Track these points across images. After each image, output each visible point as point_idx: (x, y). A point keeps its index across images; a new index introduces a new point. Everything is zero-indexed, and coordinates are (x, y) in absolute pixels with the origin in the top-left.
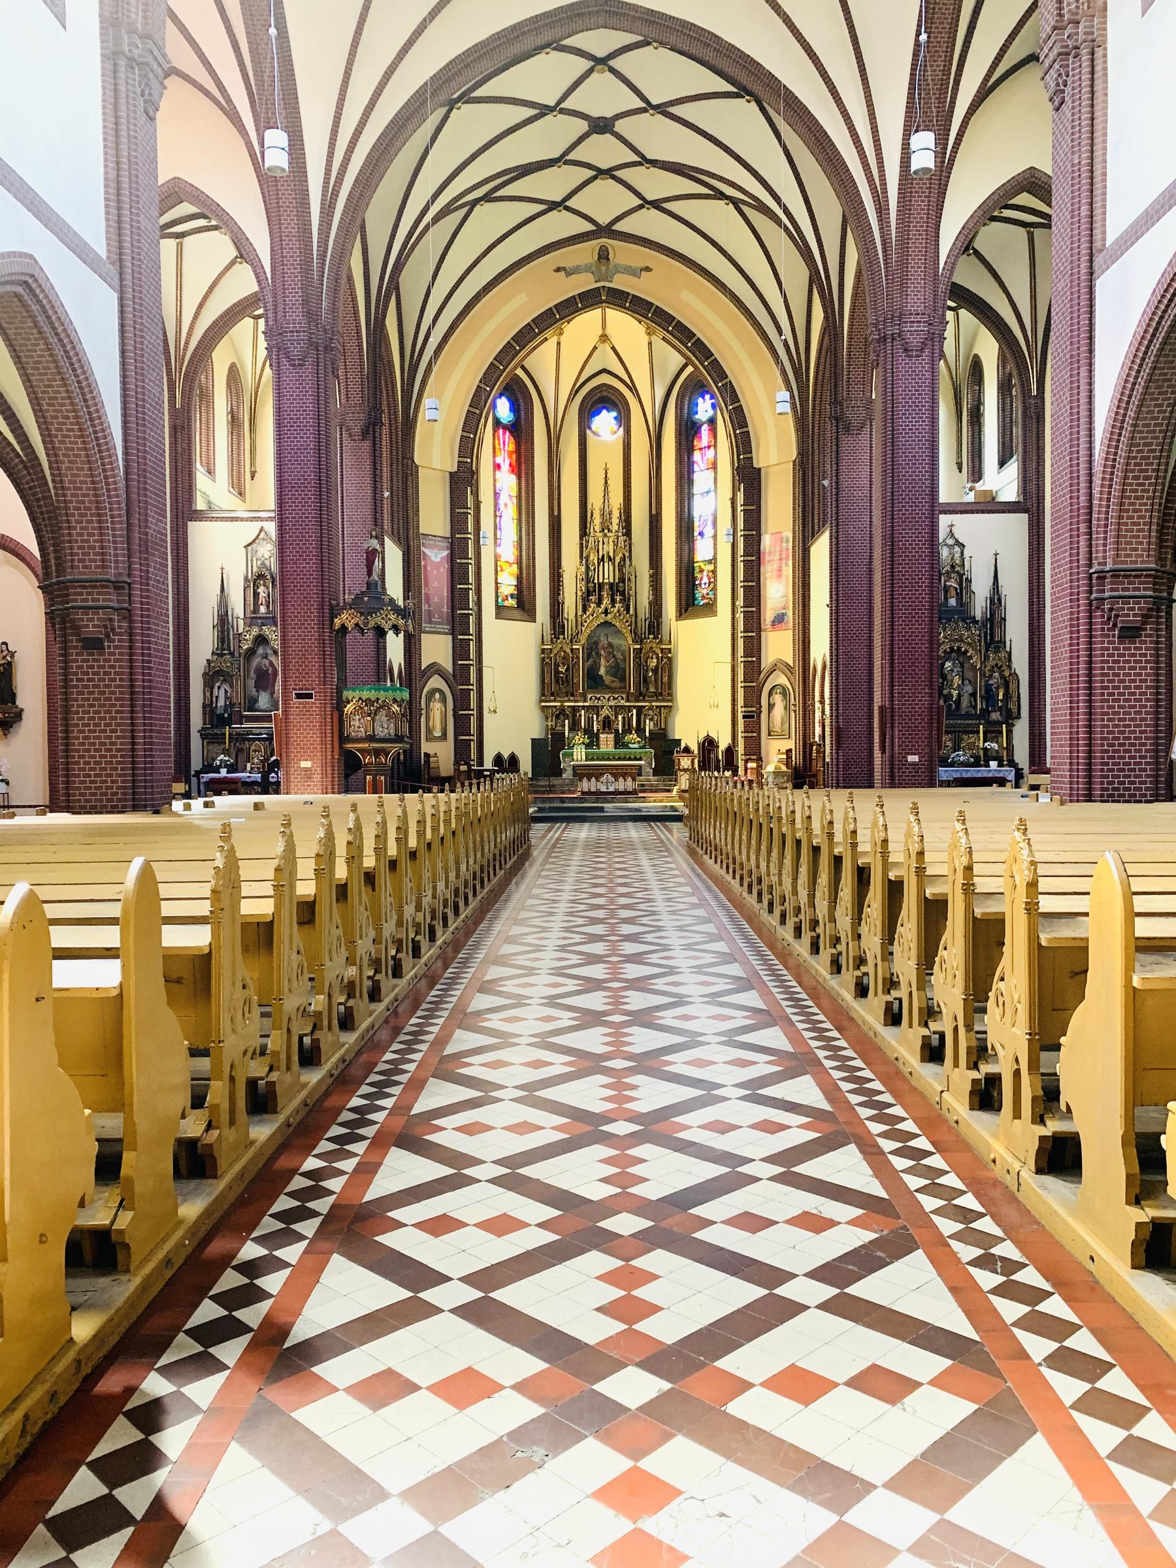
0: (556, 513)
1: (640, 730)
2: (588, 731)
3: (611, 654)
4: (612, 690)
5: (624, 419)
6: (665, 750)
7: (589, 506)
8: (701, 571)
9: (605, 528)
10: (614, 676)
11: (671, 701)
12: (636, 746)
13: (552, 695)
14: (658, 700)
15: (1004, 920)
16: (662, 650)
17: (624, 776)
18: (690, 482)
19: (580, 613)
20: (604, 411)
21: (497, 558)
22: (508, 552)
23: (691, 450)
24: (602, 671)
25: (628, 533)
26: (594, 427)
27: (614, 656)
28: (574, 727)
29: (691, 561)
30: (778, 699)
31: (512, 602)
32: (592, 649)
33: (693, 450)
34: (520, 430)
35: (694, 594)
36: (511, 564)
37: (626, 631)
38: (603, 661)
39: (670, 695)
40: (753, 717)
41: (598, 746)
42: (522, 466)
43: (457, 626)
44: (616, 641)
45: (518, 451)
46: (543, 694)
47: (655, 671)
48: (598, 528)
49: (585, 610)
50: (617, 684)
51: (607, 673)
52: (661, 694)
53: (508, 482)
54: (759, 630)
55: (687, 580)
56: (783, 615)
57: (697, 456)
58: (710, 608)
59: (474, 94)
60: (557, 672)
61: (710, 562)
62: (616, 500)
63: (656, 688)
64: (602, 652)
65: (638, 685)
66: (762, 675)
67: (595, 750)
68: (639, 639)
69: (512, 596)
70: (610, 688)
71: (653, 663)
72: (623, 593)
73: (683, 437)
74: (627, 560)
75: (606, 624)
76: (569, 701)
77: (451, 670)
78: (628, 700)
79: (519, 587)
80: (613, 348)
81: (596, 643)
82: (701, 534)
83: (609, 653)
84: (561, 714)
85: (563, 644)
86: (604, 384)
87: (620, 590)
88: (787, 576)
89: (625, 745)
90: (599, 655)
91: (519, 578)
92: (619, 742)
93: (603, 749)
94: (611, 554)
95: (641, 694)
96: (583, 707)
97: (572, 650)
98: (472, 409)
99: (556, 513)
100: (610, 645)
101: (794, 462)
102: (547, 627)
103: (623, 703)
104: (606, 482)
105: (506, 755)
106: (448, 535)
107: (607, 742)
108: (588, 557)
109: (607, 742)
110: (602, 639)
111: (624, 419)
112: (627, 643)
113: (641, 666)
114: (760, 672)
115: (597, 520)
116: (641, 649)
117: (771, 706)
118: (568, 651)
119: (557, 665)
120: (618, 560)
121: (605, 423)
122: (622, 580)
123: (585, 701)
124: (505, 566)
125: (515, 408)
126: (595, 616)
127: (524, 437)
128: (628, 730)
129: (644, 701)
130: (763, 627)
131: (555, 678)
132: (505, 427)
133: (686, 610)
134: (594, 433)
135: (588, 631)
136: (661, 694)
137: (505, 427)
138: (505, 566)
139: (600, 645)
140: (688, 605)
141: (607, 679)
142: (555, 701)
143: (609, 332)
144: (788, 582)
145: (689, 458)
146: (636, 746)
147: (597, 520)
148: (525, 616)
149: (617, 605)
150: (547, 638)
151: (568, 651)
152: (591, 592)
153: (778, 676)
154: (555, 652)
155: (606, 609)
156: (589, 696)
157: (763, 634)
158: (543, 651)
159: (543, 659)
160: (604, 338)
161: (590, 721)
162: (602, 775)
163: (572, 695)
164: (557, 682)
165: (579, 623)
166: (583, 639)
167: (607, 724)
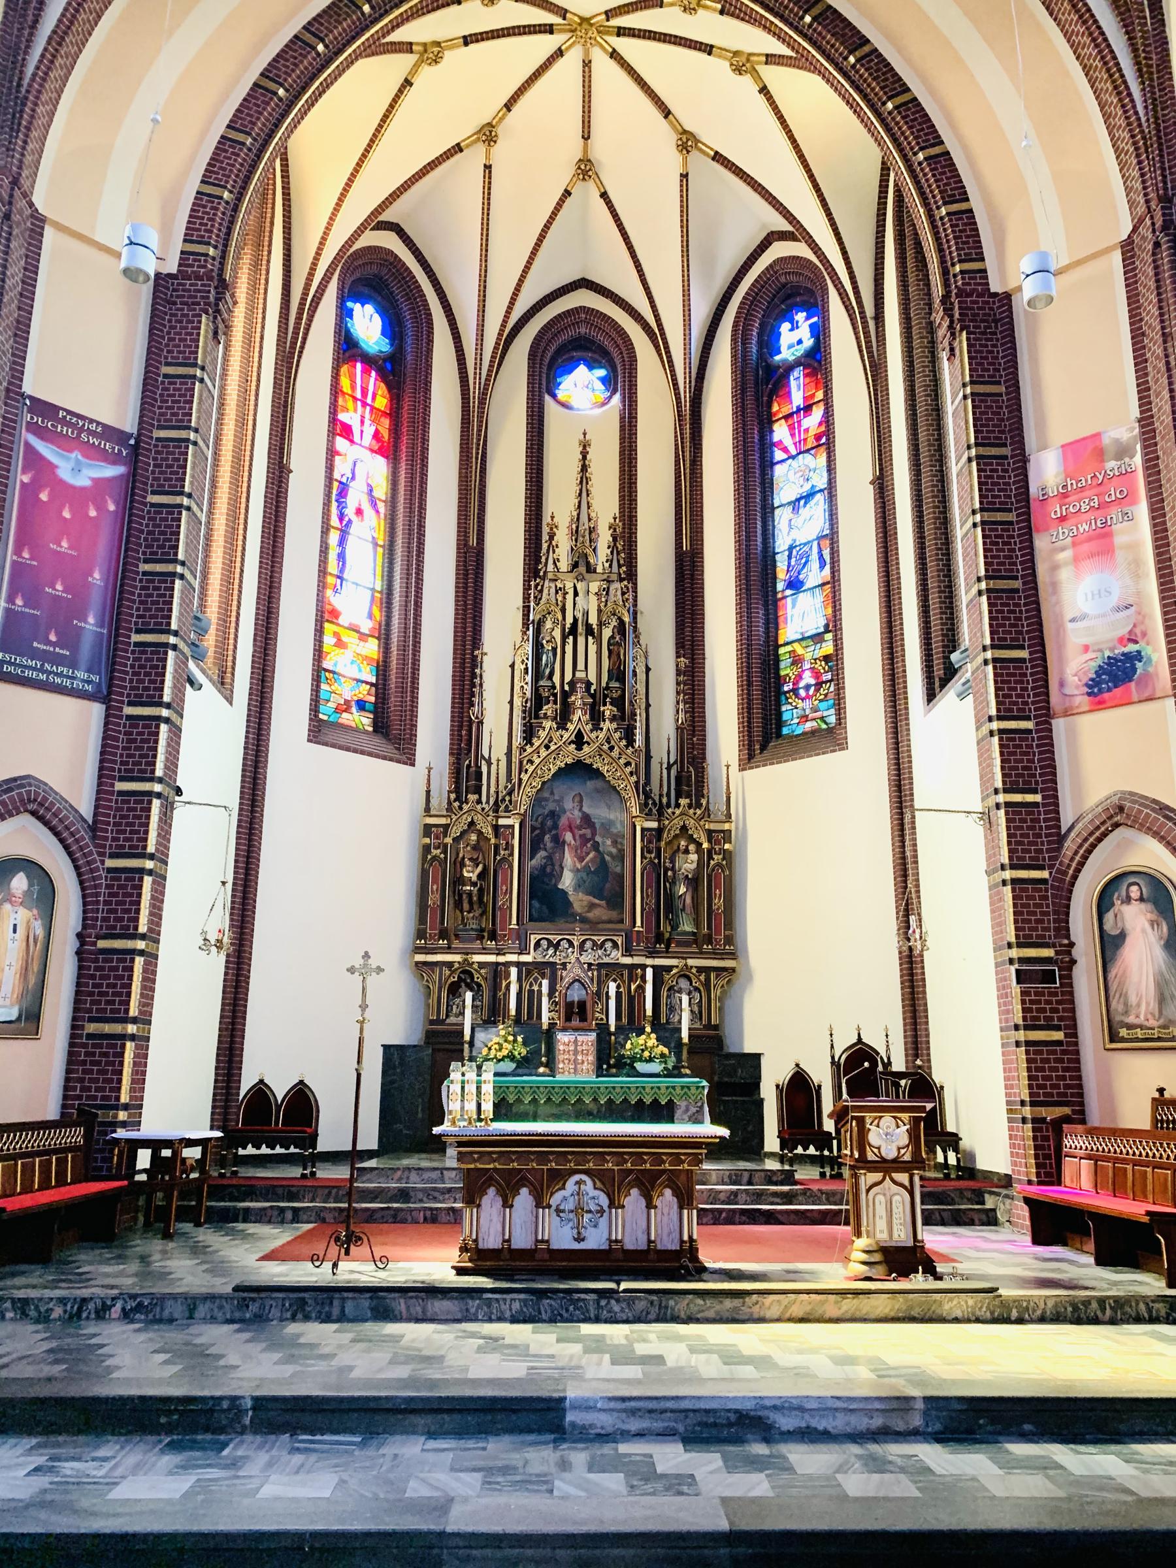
0: (473, 541)
1: (666, 1031)
2: (526, 1022)
3: (588, 842)
4: (592, 926)
5: (622, 377)
6: (731, 1079)
7: (546, 519)
8: (797, 661)
9: (582, 564)
10: (596, 891)
11: (733, 955)
12: (655, 1067)
13: (443, 934)
14: (701, 954)
15: (672, 1121)
16: (710, 833)
17: (648, 1185)
18: (767, 486)
19: (518, 740)
20: (582, 369)
21: (325, 615)
22: (356, 603)
23: (766, 422)
24: (567, 881)
25: (631, 575)
26: (561, 394)
27: (596, 847)
28: (492, 1014)
29: (771, 645)
30: (1135, 918)
31: (364, 721)
32: (543, 829)
33: (771, 422)
34: (403, 372)
35: (779, 714)
36: (363, 637)
37: (626, 786)
38: (569, 859)
39: (729, 940)
40: (1048, 977)
41: (551, 1065)
42: (404, 440)
43: (126, 680)
44: (600, 812)
45: (394, 413)
46: (421, 934)
47: (694, 882)
48: (564, 565)
49: (529, 734)
50: (601, 912)
51: (578, 886)
52: (709, 939)
53: (367, 471)
54: (1045, 716)
55: (765, 680)
56: (1133, 658)
57: (780, 432)
58: (830, 737)
59: (390, 38)
60: (459, 880)
61: (818, 638)
62: (606, 507)
63: (697, 923)
64: (568, 837)
65: (653, 915)
66: (1069, 845)
67: (540, 1077)
68: (653, 806)
69: (361, 705)
70: (584, 920)
71: (689, 863)
72: (619, 703)
73: (750, 394)
74: (630, 636)
75: (579, 770)
76: (485, 951)
77: (86, 808)
78: (628, 952)
79: (381, 686)
80: (604, 195)
81: (553, 815)
82: (795, 585)
83: (584, 840)
84: (465, 978)
85: (478, 812)
86: (583, 309)
87: (616, 699)
88: (1134, 547)
89: (625, 1065)
90: (559, 843)
91: (382, 669)
92: (609, 1058)
93: (565, 1075)
94: (593, 620)
95: (659, 938)
96: (518, 964)
97: (496, 828)
98: (233, 135)
99: (473, 541)
100: (587, 820)
101: (1128, 248)
102: (442, 784)
103: (617, 956)
104: (584, 468)
105: (280, 1089)
106: (128, 423)
107: (575, 1055)
108: (539, 625)
109: (575, 1055)
110: (569, 804)
111: (622, 377)
112: (627, 817)
113: (659, 875)
114: (1061, 839)
115: (563, 541)
116: (660, 831)
117: (1110, 945)
118: (488, 831)
119: (459, 864)
120: (607, 633)
121: (582, 386)
122: (618, 674)
123: (523, 950)
124: (349, 637)
125: (393, 329)
126: (554, 748)
127: (408, 389)
128: (632, 1024)
129: (667, 954)
130: (1055, 699)
131: (454, 895)
132: (369, 361)
133: (763, 748)
134: (565, 405)
135: (537, 783)
136: (709, 939)
137: (369, 361)
138: (349, 637)
139: (563, 821)
140: (765, 736)
141: (579, 902)
142: (449, 950)
143: (600, 149)
144: (1137, 563)
145: (762, 438)
146: (655, 1067)
147: (563, 541)
148: (389, 749)
149: (606, 725)
150: (439, 800)
151: (488, 831)
152: (543, 702)
153: (1126, 845)
154: (455, 831)
155: (579, 735)
156: (533, 939)
157: (1059, 725)
158: (427, 830)
159: (426, 849)
160: (586, 169)
161: (530, 1001)
162: (558, 1178)
163: (493, 936)
164: (458, 905)
165: (515, 765)
166: (523, 801)
167: (576, 1013)
